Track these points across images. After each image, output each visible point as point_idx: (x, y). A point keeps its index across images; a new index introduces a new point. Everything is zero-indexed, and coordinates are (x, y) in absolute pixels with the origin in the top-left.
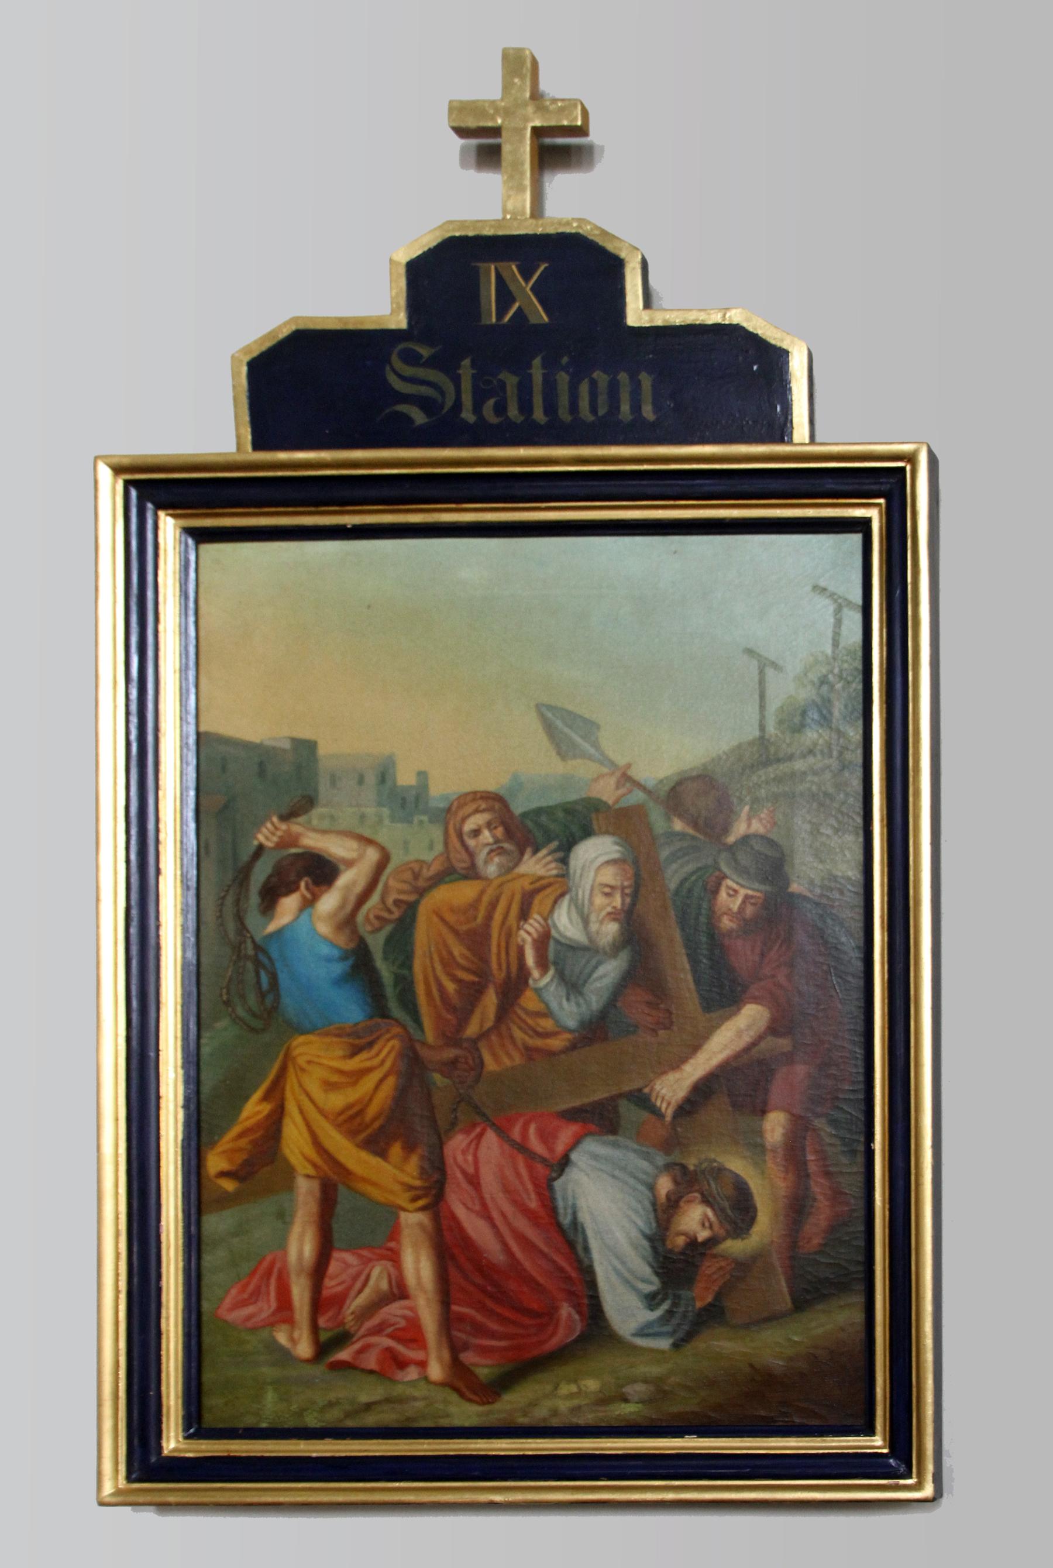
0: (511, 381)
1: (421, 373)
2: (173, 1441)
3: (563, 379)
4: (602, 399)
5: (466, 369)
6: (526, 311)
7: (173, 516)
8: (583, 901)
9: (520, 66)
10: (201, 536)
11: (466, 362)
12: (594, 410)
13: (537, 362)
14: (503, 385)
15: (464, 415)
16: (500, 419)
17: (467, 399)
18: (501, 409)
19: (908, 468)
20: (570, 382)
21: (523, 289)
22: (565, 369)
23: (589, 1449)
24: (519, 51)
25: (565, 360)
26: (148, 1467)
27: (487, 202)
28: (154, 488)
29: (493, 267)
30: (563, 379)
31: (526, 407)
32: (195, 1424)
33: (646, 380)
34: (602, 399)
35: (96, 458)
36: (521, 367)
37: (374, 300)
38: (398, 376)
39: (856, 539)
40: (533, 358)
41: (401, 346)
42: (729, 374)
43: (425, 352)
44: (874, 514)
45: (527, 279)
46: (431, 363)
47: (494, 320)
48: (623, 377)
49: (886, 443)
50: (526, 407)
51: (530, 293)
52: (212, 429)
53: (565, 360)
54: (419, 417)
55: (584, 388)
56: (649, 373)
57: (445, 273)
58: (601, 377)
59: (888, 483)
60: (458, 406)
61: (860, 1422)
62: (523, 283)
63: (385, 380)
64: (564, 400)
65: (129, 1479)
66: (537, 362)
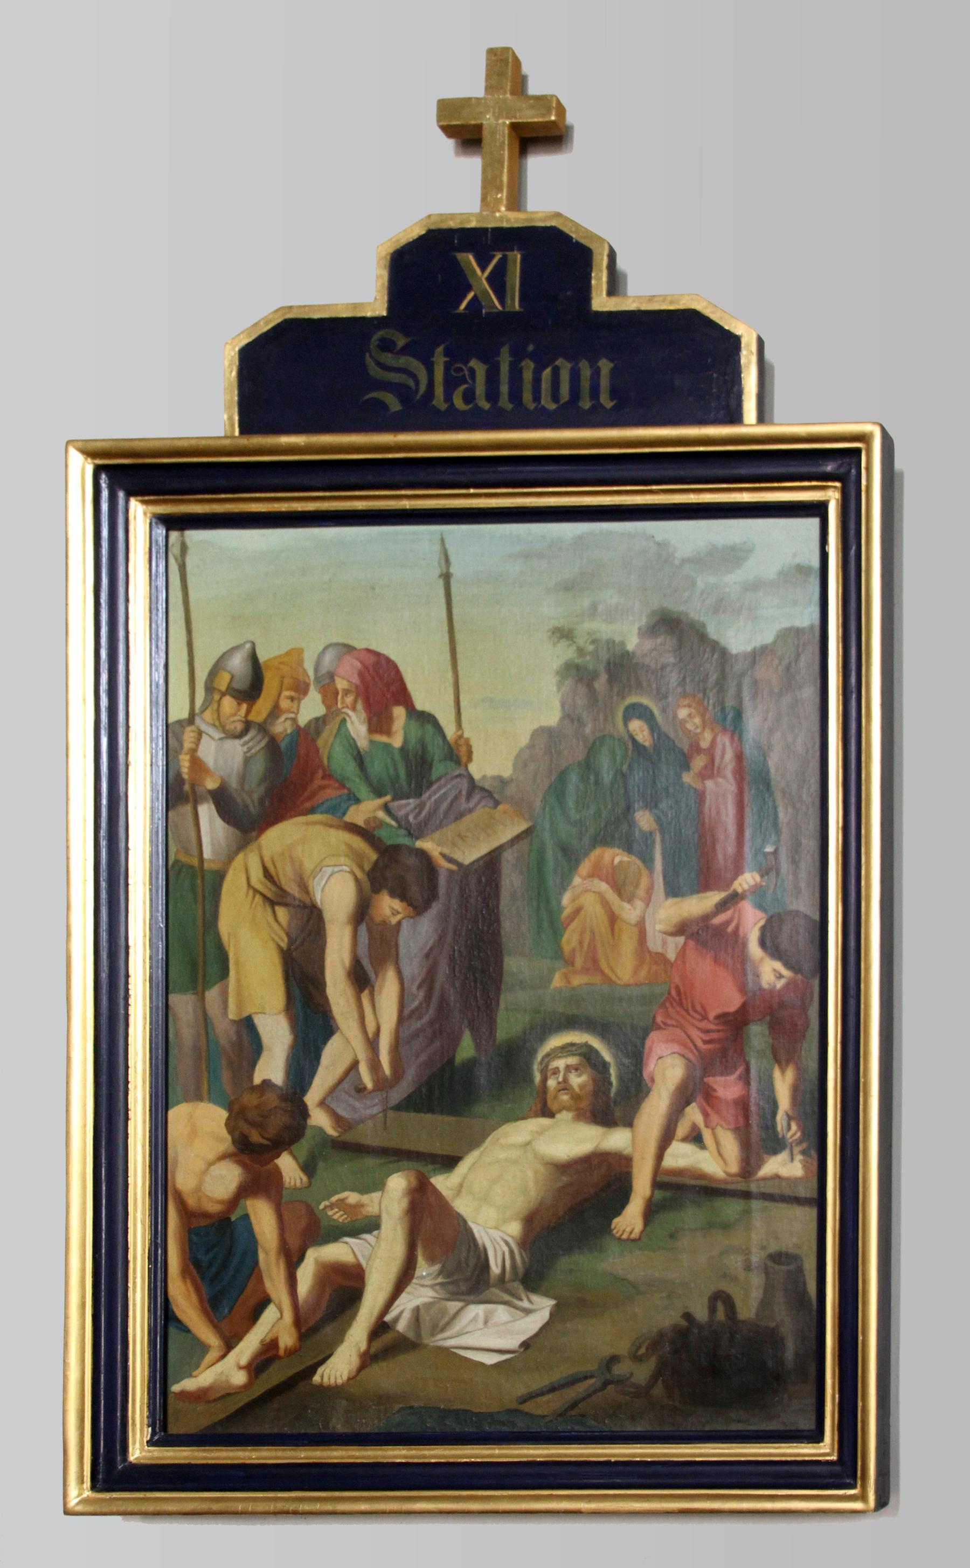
2: (139, 1449)
3: (528, 368)
4: (545, 385)
5: (440, 360)
6: (480, 298)
7: (143, 502)
9: (504, 67)
10: (172, 523)
11: (440, 350)
14: (472, 372)
16: (470, 406)
17: (439, 391)
18: (469, 397)
21: (480, 279)
23: (144, 1090)
25: (531, 348)
26: (112, 1474)
27: (455, 191)
28: (129, 473)
31: (493, 394)
33: (605, 366)
34: (545, 385)
35: (68, 443)
37: (361, 290)
38: (385, 365)
39: (815, 522)
40: (439, 345)
41: (381, 333)
42: (686, 358)
44: (832, 497)
45: (483, 269)
46: (405, 351)
49: (789, 424)
50: (493, 394)
51: (485, 282)
52: (203, 412)
53: (531, 348)
54: (394, 405)
56: (612, 360)
57: (425, 265)
58: (565, 367)
59: (836, 461)
60: (430, 393)
61: (173, 1429)
63: (364, 367)
65: (94, 1487)
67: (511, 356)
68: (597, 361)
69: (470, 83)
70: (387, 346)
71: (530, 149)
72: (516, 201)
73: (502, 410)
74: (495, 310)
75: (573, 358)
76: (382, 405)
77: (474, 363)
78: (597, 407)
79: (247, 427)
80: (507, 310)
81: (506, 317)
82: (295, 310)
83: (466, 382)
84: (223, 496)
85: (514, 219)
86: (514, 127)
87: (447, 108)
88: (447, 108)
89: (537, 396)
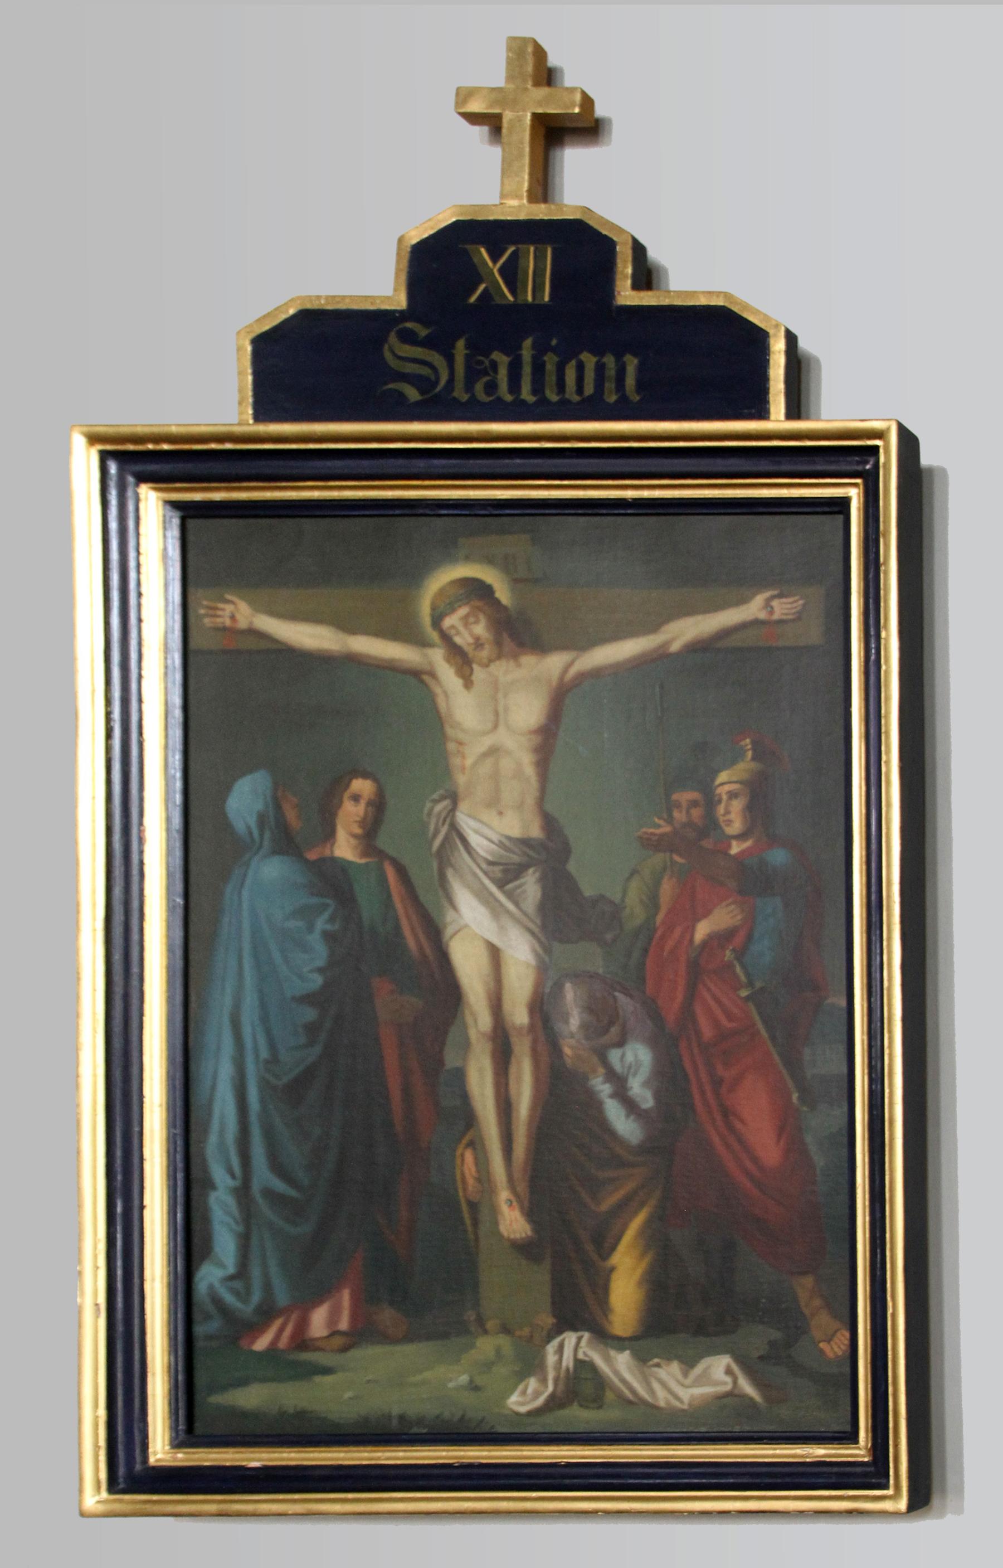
0: (502, 360)
1: (418, 352)
3: (551, 361)
5: (460, 346)
6: (492, 292)
7: (155, 489)
8: (421, 948)
12: (580, 389)
13: (528, 343)
14: (494, 366)
15: (456, 394)
18: (491, 387)
19: (887, 1506)
20: (453, 390)
21: (492, 270)
22: (554, 350)
24: (525, 41)
25: (554, 342)
26: (129, 1473)
27: (484, 183)
28: (135, 460)
29: (532, 249)
30: (551, 361)
32: (188, 1430)
33: (632, 363)
34: (590, 376)
36: (513, 350)
37: (379, 283)
38: (397, 352)
40: (524, 339)
42: (717, 355)
43: (423, 332)
44: (854, 494)
45: (495, 261)
46: (428, 343)
47: (530, 298)
48: (609, 360)
50: (514, 385)
52: (218, 401)
53: (554, 342)
54: (413, 394)
55: (589, 389)
57: (441, 260)
58: (589, 360)
61: (848, 1428)
62: (490, 264)
64: (551, 378)
66: (528, 343)
67: (467, 348)
68: (623, 355)
69: (491, 71)
70: (408, 337)
71: (567, 139)
72: (543, 185)
73: (523, 402)
74: (504, 302)
75: (598, 351)
76: (401, 395)
77: (496, 356)
78: (623, 399)
79: (259, 416)
80: (520, 302)
81: (519, 309)
82: (347, 300)
83: (487, 374)
84: (284, 484)
85: (541, 212)
86: (536, 117)
87: (463, 95)
88: (463, 95)
89: (600, 368)
